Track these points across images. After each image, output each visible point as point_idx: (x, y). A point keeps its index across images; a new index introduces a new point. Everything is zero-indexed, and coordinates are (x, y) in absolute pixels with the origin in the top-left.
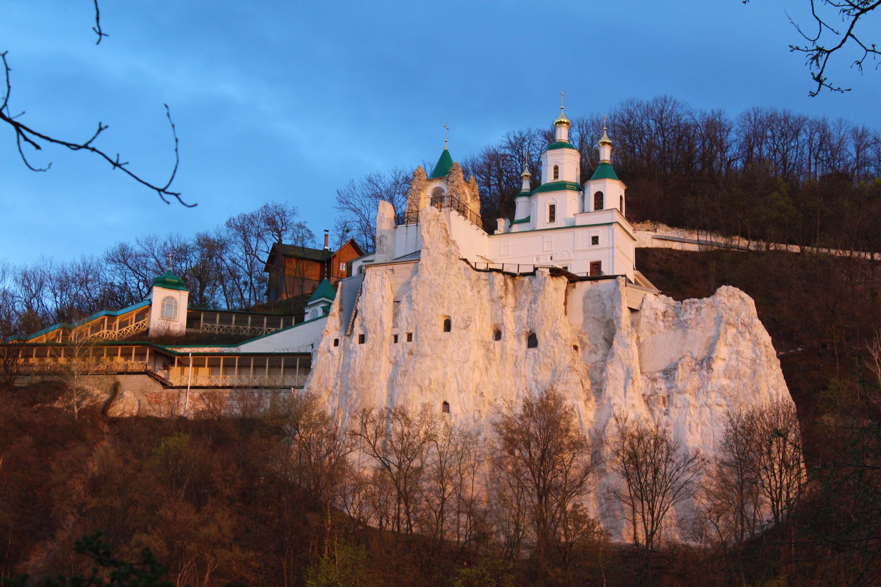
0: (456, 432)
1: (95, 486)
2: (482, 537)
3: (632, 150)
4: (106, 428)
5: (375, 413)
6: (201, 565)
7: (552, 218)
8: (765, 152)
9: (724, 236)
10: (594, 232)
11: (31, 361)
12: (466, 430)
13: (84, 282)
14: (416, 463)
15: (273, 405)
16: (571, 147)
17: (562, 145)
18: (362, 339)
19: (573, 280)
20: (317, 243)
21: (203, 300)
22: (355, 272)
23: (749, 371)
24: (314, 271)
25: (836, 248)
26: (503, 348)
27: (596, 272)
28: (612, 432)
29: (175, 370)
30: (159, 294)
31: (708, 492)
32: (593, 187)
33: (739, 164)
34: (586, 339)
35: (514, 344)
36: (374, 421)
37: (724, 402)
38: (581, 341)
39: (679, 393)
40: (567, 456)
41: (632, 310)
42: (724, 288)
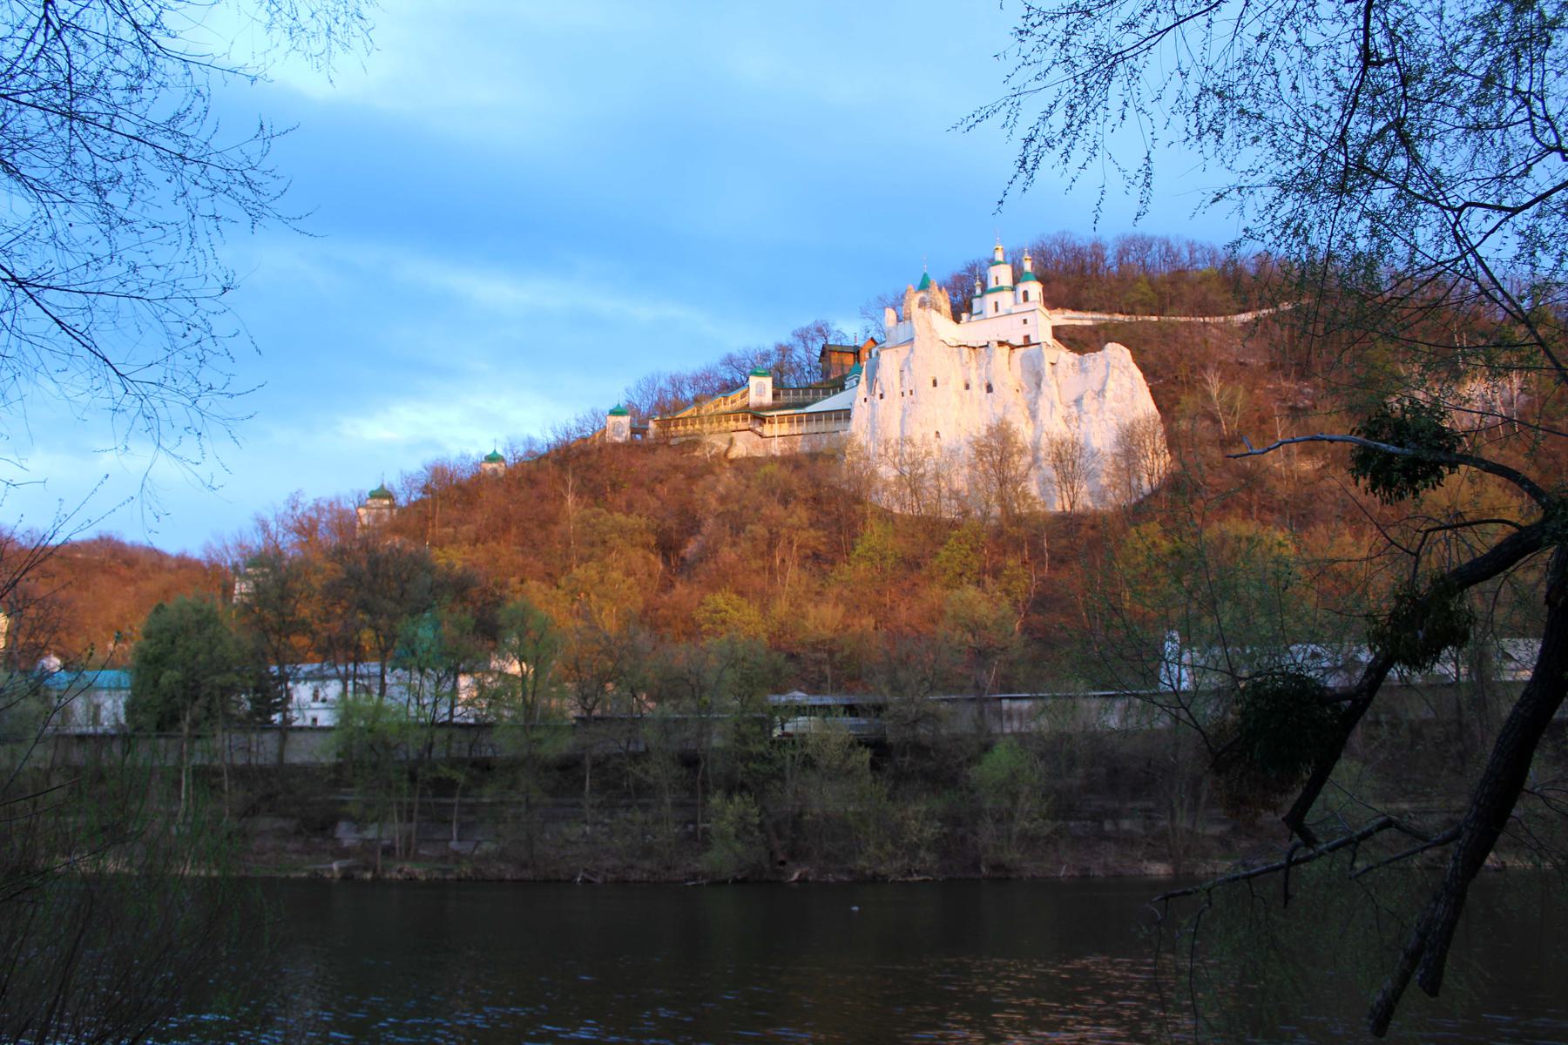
0: (945, 450)
1: (722, 500)
2: (966, 513)
3: (1046, 266)
4: (728, 465)
5: (892, 441)
6: (791, 543)
7: (997, 310)
8: (1131, 259)
9: (1108, 314)
11: (679, 428)
12: (951, 448)
13: (707, 379)
14: (921, 471)
15: (829, 442)
16: (1005, 263)
17: (999, 263)
18: (882, 396)
19: (1013, 347)
20: (850, 342)
21: (782, 384)
22: (874, 355)
23: (1129, 396)
24: (849, 359)
25: (1180, 316)
26: (971, 395)
27: (1027, 342)
28: (1044, 441)
29: (767, 426)
30: (753, 381)
31: (1108, 474)
32: (1021, 287)
33: (1115, 268)
34: (1024, 385)
35: (978, 391)
36: (892, 447)
37: (1114, 417)
38: (1021, 386)
39: (1085, 413)
40: (1016, 458)
41: (1052, 364)
42: (1109, 344)
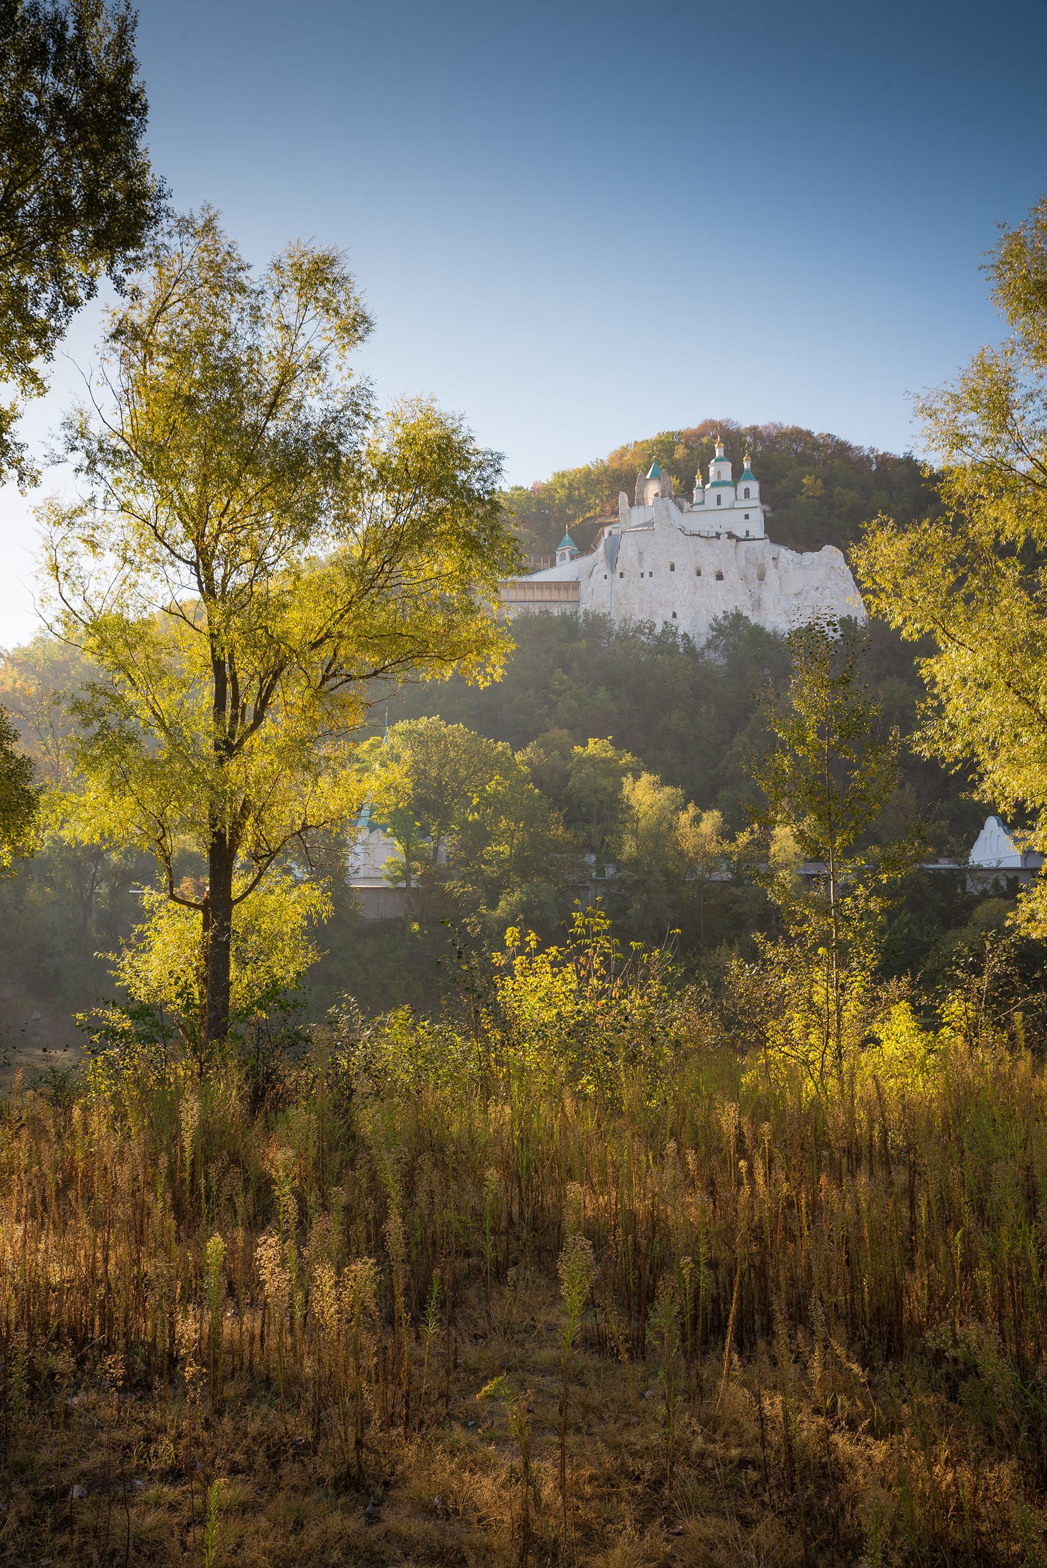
10: (747, 512)
18: (622, 575)
19: (739, 540)
32: (742, 486)
